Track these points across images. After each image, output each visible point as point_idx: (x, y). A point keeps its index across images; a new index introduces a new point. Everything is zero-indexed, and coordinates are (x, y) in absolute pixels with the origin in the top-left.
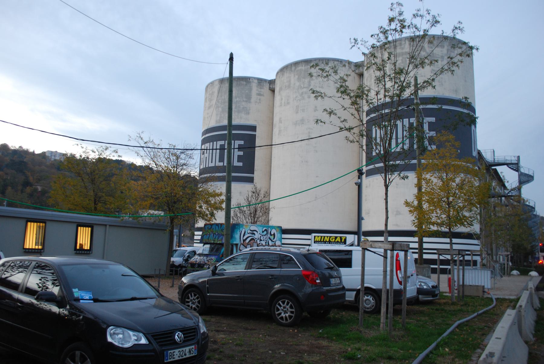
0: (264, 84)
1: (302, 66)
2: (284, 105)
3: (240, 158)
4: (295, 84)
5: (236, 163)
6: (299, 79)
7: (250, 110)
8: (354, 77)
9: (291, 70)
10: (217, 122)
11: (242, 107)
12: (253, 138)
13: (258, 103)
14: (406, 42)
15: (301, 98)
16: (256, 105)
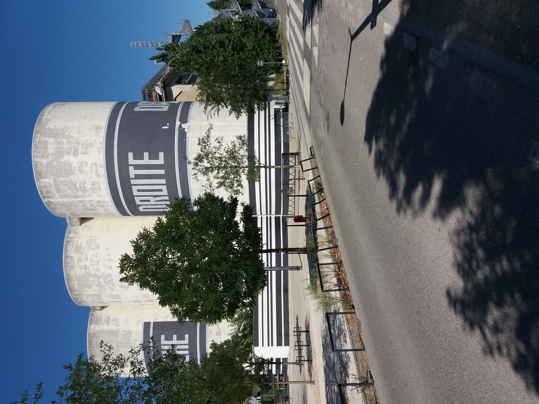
0: (96, 316)
1: (74, 284)
2: (120, 299)
3: (154, 156)
4: (95, 290)
5: (161, 161)
7: (126, 331)
8: (85, 226)
9: (79, 294)
11: (122, 340)
12: (157, 325)
13: (118, 322)
14: (43, 182)
15: (110, 284)
16: (120, 325)
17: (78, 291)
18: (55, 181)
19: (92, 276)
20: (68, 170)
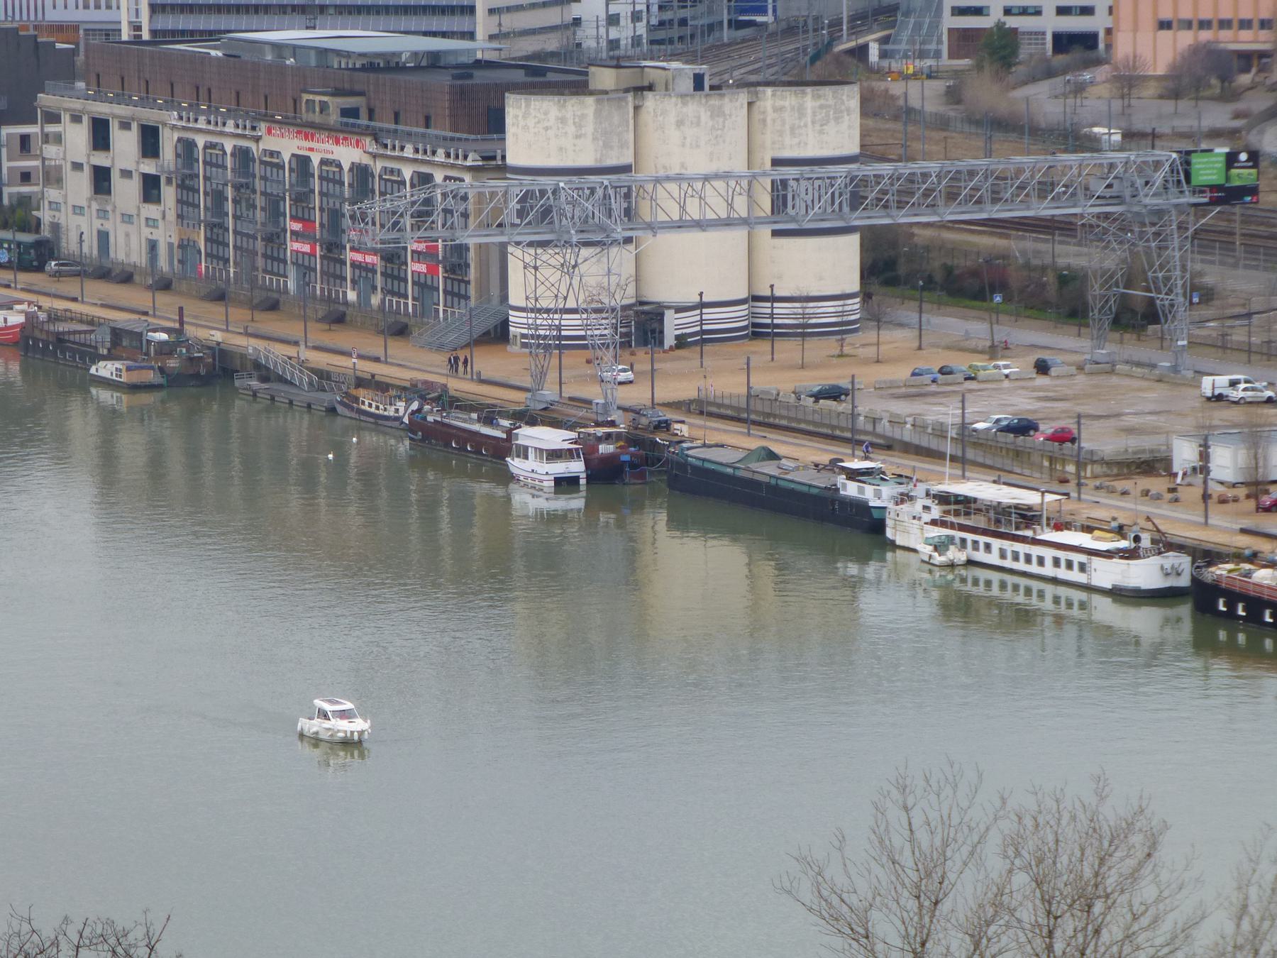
6: (712, 117)
10: (596, 160)
17: (707, 102)
18: (829, 106)
19: (724, 122)
20: (837, 120)
